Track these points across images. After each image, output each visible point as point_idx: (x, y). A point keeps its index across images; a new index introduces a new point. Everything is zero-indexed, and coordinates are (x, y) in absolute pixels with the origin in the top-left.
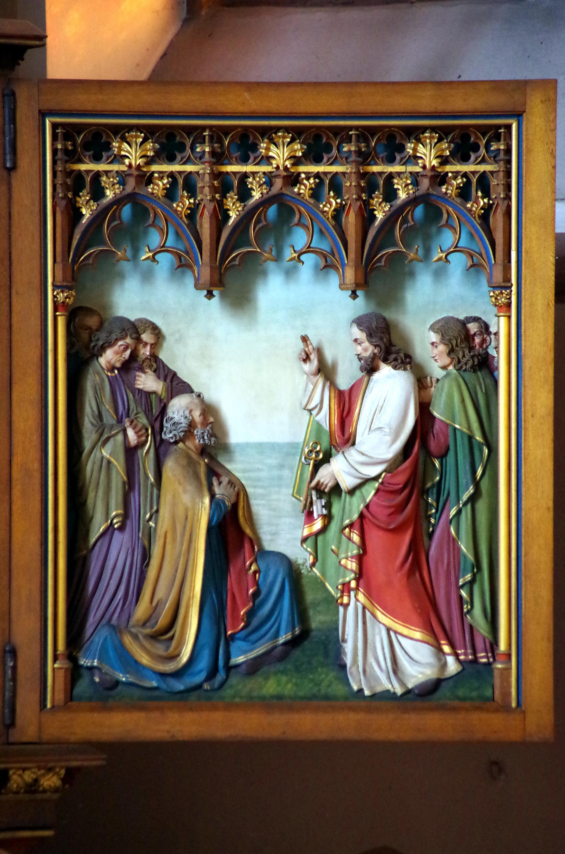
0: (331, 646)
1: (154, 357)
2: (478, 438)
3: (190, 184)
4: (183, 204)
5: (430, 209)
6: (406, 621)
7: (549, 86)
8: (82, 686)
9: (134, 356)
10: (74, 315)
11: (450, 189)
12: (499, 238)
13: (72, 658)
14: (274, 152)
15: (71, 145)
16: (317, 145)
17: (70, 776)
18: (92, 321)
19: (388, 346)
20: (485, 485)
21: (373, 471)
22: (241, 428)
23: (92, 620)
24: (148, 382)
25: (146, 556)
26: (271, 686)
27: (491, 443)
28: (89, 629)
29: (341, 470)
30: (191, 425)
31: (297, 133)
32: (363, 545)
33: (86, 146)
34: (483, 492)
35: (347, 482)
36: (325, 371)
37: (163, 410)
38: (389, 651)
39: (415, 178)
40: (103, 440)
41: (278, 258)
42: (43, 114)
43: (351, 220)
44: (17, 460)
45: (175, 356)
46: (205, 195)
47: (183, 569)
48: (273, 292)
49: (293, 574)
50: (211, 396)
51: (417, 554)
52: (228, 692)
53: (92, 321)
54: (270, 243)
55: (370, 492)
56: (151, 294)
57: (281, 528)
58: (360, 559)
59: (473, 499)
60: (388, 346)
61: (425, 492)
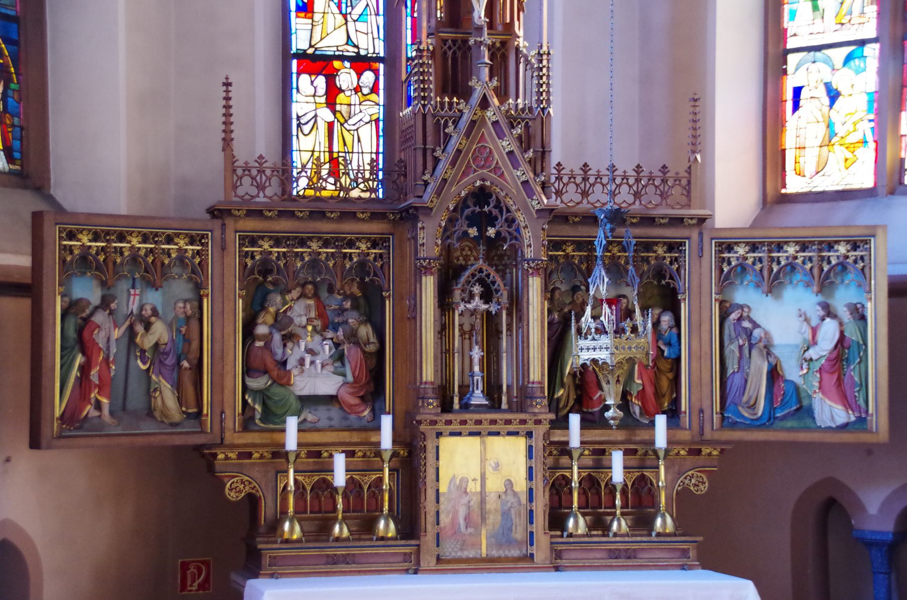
1: (748, 316)
2: (861, 342)
3: (760, 260)
4: (758, 266)
5: (843, 267)
6: (836, 403)
7: (884, 227)
8: (726, 423)
9: (741, 316)
10: (722, 303)
11: (850, 260)
12: (868, 276)
13: (722, 414)
14: (789, 249)
16: (804, 247)
17: (722, 451)
18: (728, 305)
20: (863, 359)
21: (824, 353)
23: (729, 401)
24: (746, 324)
25: (746, 381)
26: (789, 424)
27: (865, 344)
28: (727, 404)
29: (812, 353)
30: (761, 338)
31: (797, 243)
32: (821, 378)
33: (726, 249)
34: (864, 360)
35: (815, 357)
36: (807, 320)
37: (751, 334)
38: (830, 412)
39: (838, 257)
40: (731, 342)
41: (791, 282)
42: (712, 239)
44: (703, 350)
46: (765, 263)
47: (759, 386)
49: (797, 388)
51: (839, 382)
52: (775, 426)
53: (728, 305)
54: (788, 278)
55: (823, 361)
56: (745, 295)
57: (792, 372)
58: (820, 382)
59: (859, 363)
60: (829, 312)
61: (842, 360)
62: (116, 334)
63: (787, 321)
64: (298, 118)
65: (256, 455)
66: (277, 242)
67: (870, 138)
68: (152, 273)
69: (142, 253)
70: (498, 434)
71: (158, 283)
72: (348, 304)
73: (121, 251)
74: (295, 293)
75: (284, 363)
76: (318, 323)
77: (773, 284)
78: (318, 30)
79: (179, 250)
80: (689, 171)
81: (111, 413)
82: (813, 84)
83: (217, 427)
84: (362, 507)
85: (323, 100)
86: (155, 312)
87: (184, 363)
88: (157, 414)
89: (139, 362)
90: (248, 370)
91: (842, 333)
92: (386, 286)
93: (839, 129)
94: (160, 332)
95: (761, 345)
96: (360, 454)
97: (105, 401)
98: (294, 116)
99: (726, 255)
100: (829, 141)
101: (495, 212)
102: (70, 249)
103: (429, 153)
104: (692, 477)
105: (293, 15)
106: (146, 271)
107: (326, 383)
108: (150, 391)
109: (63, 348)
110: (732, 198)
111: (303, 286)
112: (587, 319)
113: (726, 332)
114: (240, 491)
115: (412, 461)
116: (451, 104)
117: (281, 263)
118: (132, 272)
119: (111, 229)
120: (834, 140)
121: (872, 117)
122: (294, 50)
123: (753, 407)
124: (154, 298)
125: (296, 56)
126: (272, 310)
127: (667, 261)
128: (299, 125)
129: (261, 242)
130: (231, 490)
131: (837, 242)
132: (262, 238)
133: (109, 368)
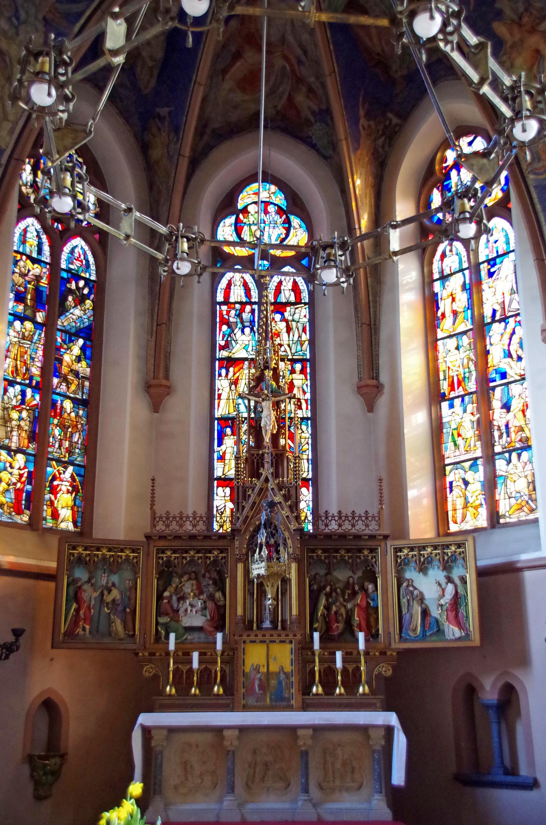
0: (443, 632)
3: (415, 555)
15: (392, 655)
19: (449, 580)
22: (427, 596)
24: (411, 588)
29: (442, 602)
35: (443, 603)
38: (453, 631)
43: (441, 559)
45: (415, 584)
48: (431, 572)
49: (437, 621)
50: (421, 590)
51: (456, 616)
57: (435, 612)
58: (447, 616)
60: (449, 580)
62: (96, 594)
63: (430, 585)
64: (217, 507)
65: (158, 654)
66: (175, 552)
67: (483, 503)
68: (113, 566)
69: (108, 556)
70: (274, 642)
71: (115, 571)
72: (211, 582)
73: (97, 556)
74: (186, 577)
75: (178, 611)
76: (197, 592)
77: (423, 569)
78: (227, 467)
79: (127, 556)
80: (379, 513)
81: (90, 633)
82: (457, 479)
83: (142, 641)
84: (206, 678)
85: (229, 498)
86: (114, 585)
87: (127, 610)
88: (113, 635)
89: (106, 609)
90: (159, 613)
91: (457, 592)
92: (226, 571)
93: (471, 500)
94: (115, 594)
95: (418, 598)
96: (209, 654)
97: (88, 627)
98: (215, 506)
99: (399, 554)
100: (465, 507)
101: (274, 532)
102: (73, 554)
103: (240, 504)
104: (383, 667)
105: (215, 461)
106: (110, 565)
107: (198, 621)
108: (110, 623)
109: (67, 600)
110: (420, 524)
111: (190, 574)
112: (256, 556)
113: (401, 593)
114: (150, 672)
115: (232, 654)
116: (251, 481)
117: (176, 561)
118: (103, 566)
119: (115, 546)
120: (469, 505)
121: (483, 492)
122: (215, 477)
123: (415, 630)
124: (115, 578)
125: (216, 479)
126: (174, 585)
127: (370, 558)
128: (217, 510)
129: (166, 552)
130: (146, 671)
131: (451, 545)
132: (167, 549)
133: (90, 611)
